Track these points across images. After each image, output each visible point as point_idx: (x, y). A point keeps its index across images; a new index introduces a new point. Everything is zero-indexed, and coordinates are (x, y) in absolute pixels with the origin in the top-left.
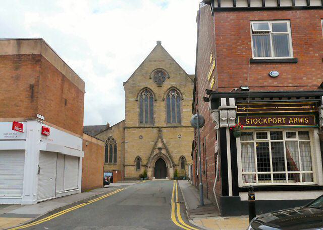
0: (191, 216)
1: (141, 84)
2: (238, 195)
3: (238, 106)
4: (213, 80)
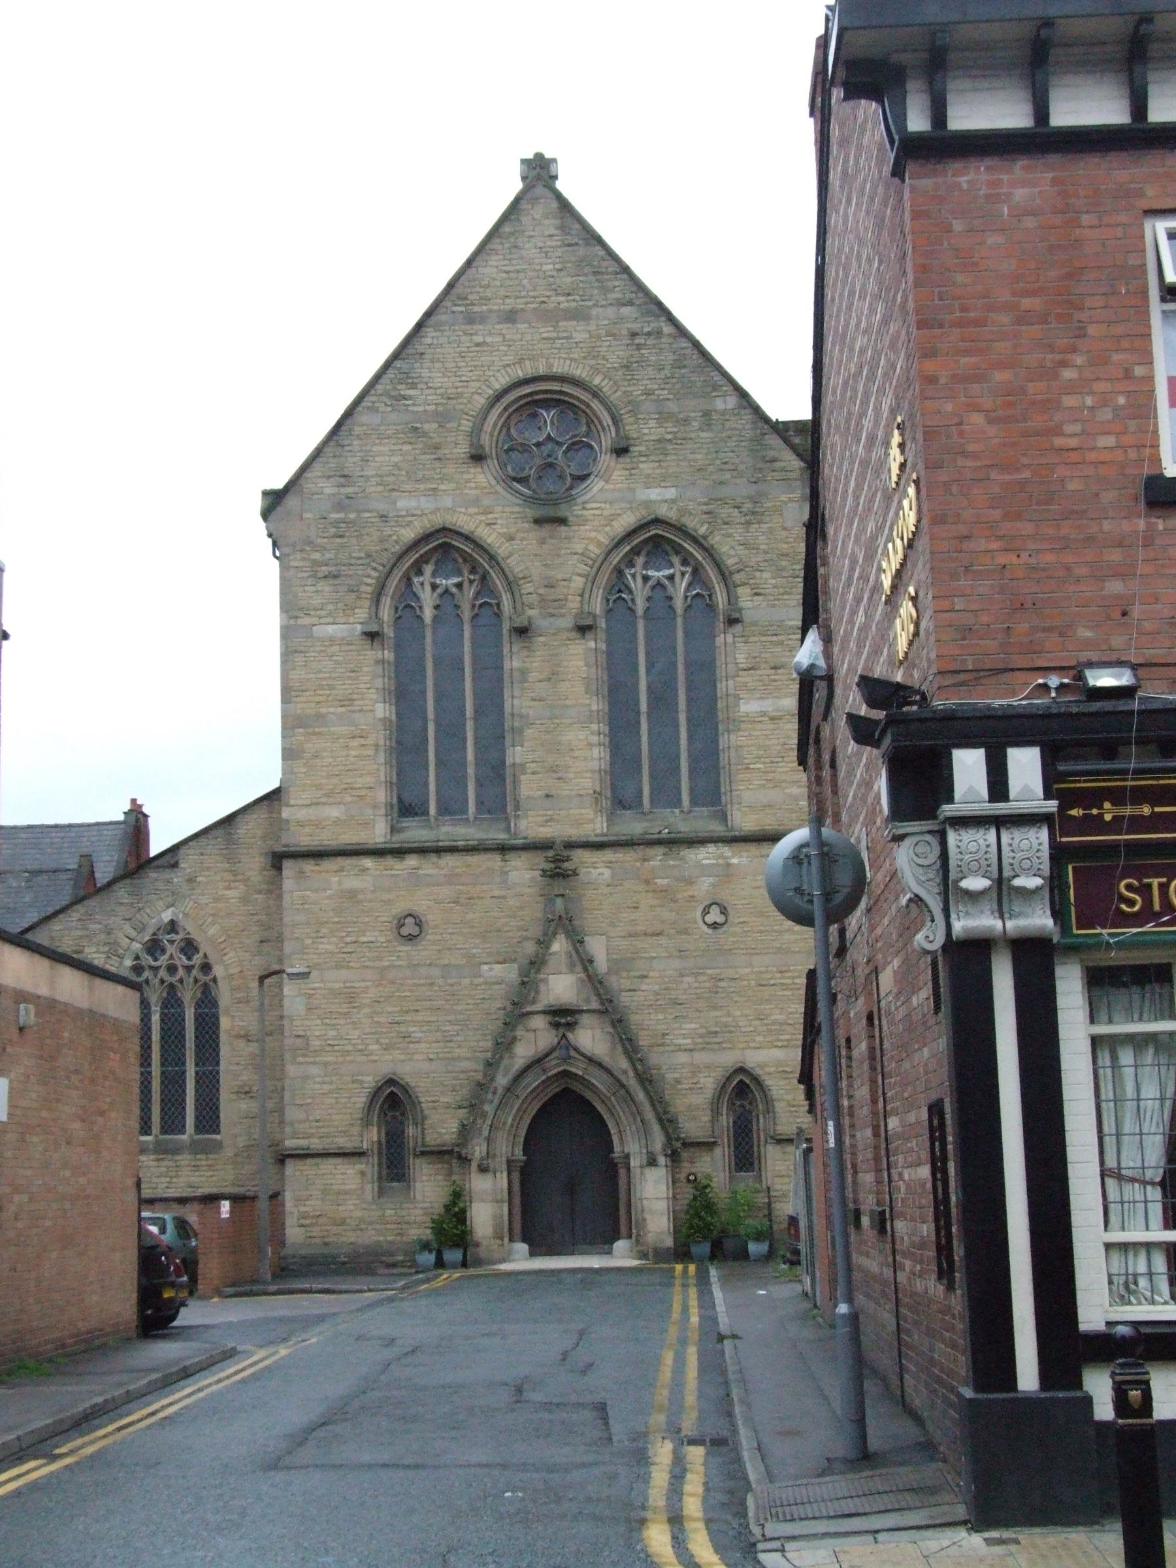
0: (772, 1529)
1: (404, 503)
2: (1079, 1385)
3: (1067, 799)
4: (907, 609)
